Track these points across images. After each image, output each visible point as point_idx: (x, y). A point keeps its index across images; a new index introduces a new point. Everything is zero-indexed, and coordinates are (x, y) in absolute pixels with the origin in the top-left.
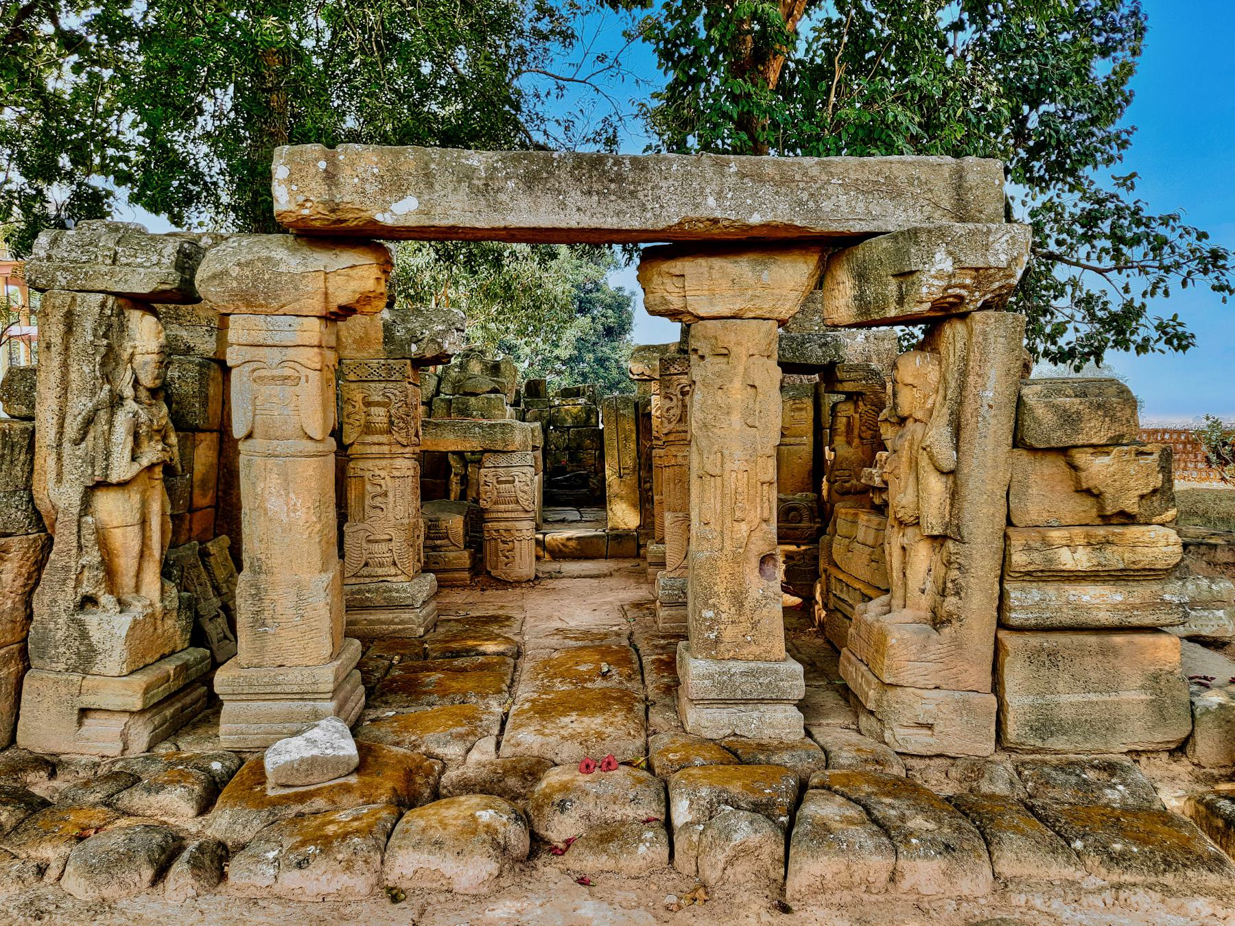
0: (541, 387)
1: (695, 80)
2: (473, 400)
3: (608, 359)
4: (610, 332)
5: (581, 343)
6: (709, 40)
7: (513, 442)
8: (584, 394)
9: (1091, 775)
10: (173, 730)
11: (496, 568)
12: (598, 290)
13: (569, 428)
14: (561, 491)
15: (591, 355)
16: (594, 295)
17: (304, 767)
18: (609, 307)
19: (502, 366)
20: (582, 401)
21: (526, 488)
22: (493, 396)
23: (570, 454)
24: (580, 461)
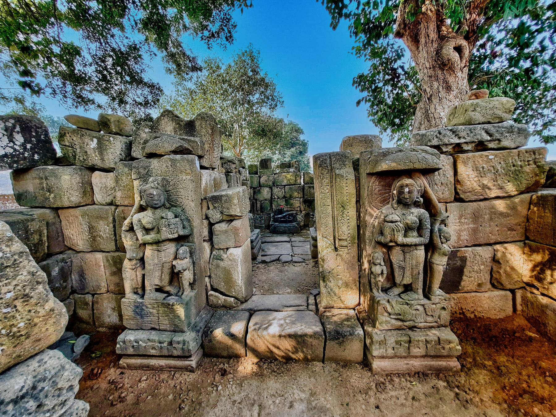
0: (268, 163)
1: (190, 61)
4: (301, 153)
6: (529, 93)
8: (293, 166)
9: (361, 321)
10: (54, 25)
13: (285, 186)
17: (402, 26)
19: (197, 124)
20: (292, 170)
22: (178, 157)
23: (286, 200)
24: (292, 204)
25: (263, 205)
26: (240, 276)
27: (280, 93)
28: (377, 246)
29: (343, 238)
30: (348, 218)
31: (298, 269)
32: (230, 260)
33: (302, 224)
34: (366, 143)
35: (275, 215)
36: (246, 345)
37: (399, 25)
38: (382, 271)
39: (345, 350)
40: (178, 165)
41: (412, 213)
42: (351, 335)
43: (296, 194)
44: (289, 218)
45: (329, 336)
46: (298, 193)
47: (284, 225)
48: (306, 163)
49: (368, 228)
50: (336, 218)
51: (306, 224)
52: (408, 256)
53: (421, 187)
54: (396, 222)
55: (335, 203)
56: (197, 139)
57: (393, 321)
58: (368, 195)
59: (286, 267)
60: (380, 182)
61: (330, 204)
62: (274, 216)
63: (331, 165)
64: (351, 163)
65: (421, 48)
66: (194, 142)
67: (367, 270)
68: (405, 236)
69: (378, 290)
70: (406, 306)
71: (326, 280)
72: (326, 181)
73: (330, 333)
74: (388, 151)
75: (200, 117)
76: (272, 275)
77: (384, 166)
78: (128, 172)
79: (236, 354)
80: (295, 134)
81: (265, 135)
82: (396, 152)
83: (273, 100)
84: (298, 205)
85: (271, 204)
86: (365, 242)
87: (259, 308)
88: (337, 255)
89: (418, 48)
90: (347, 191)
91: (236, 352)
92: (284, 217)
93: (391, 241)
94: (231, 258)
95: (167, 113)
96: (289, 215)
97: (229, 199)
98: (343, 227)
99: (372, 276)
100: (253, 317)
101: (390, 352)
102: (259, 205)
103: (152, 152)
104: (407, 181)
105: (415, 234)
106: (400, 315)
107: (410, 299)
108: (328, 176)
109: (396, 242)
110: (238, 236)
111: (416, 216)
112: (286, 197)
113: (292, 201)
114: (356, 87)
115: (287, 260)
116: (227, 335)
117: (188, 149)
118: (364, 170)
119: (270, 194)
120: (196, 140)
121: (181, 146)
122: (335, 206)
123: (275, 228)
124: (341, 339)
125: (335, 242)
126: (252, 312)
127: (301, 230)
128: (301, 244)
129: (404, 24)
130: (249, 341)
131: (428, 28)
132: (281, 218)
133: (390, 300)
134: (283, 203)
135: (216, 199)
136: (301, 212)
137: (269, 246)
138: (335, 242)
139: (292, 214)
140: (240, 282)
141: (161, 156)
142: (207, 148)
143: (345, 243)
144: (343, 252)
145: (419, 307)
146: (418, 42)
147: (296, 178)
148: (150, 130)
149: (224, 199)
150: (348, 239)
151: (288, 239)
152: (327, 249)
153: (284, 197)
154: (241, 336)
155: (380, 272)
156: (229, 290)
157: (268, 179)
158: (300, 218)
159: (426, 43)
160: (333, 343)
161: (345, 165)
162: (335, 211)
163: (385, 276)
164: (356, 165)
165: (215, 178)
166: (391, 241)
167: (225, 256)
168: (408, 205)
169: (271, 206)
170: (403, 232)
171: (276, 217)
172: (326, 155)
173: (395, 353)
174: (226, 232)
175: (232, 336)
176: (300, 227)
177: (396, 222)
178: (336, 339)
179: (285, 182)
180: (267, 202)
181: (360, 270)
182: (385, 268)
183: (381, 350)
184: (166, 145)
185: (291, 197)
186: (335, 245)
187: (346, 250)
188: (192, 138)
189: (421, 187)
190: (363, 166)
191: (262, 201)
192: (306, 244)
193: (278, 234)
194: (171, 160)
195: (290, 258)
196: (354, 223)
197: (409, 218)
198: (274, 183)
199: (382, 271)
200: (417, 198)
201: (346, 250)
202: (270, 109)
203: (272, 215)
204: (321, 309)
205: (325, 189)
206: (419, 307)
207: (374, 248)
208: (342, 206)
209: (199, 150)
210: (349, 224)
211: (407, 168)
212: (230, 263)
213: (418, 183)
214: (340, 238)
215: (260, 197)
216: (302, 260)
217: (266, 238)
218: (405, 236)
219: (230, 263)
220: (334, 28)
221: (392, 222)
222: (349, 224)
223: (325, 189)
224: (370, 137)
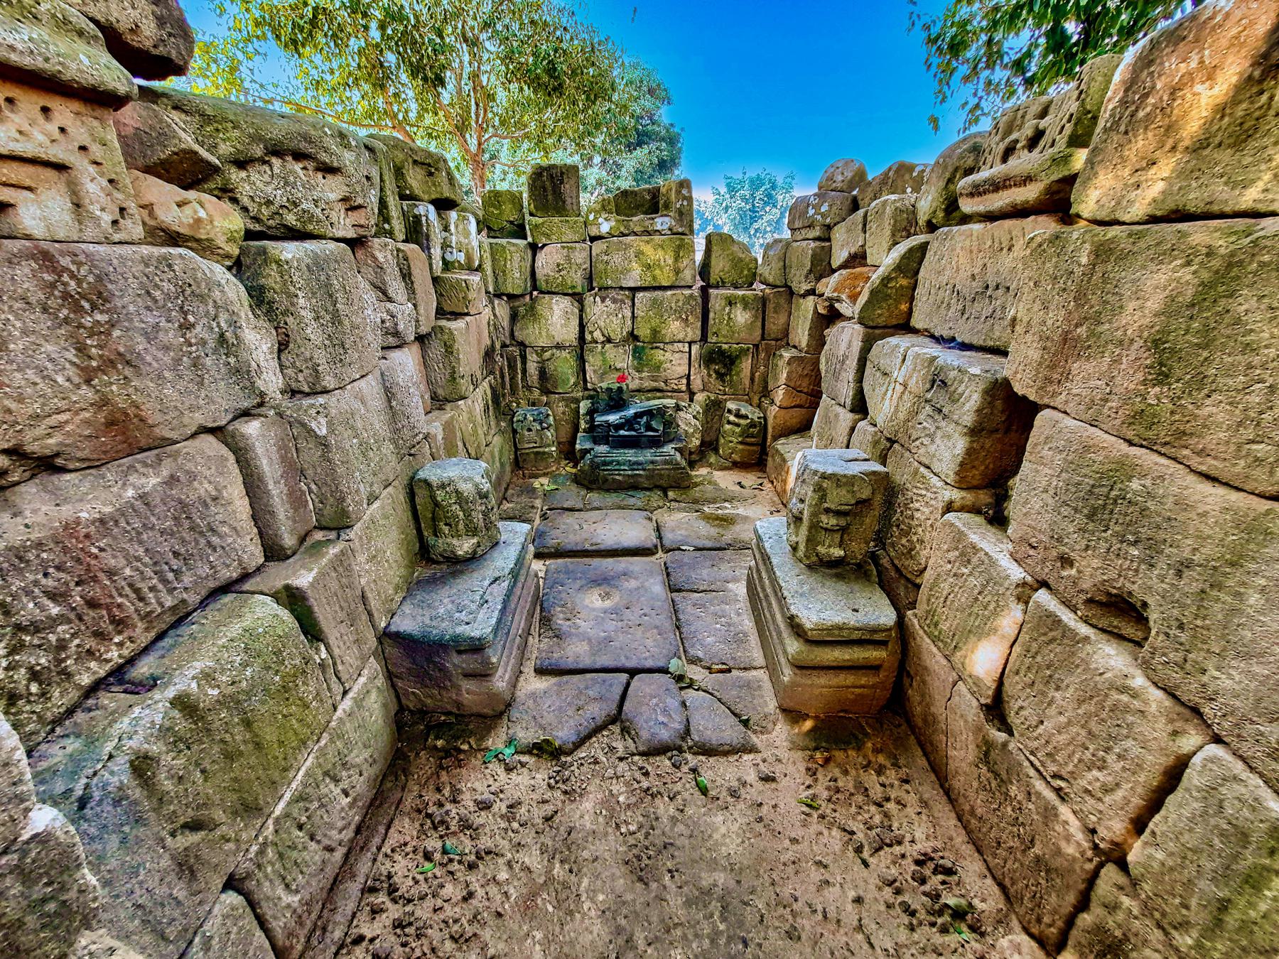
0: (567, 188)
13: (634, 290)
18: (663, 139)
25: (551, 367)
43: (674, 328)
47: (630, 455)
80: (647, 102)
81: (559, 89)
85: (582, 360)
92: (629, 423)
96: (649, 413)
102: (532, 367)
113: (659, 355)
132: (618, 427)
134: (622, 359)
139: (661, 411)
153: (633, 336)
157: (568, 258)
158: (689, 421)
171: (599, 419)
179: (634, 277)
180: (565, 354)
185: (656, 339)
191: (544, 349)
198: (590, 279)
215: (533, 334)
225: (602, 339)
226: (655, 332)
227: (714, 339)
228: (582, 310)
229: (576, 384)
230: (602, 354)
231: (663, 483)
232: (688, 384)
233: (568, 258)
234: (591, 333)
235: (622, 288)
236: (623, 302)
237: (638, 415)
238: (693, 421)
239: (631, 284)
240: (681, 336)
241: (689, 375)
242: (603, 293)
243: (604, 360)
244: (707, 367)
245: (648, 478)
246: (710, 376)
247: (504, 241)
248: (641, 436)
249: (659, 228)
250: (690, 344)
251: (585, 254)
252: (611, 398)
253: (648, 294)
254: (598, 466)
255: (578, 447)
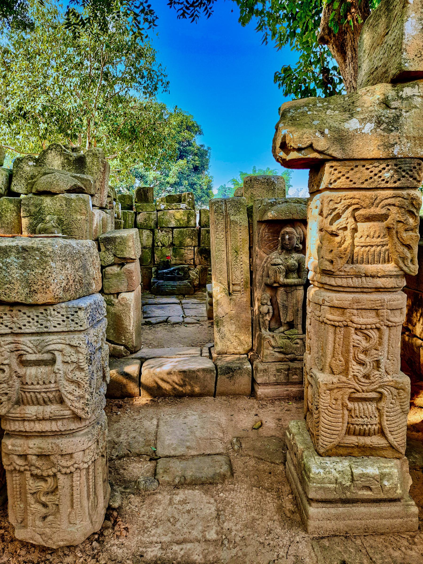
0: (149, 194)
2: (47, 201)
3: (195, 184)
5: (181, 175)
7: (46, 286)
11: (23, 524)
12: (190, 146)
13: (173, 228)
14: (166, 283)
15: (186, 182)
16: (188, 148)
17: (327, 31)
18: (196, 154)
19: (88, 160)
20: (183, 206)
21: (79, 375)
22: (73, 196)
24: (182, 255)
26: (132, 321)
27: (163, 67)
28: (267, 289)
29: (237, 283)
30: (241, 263)
31: (191, 329)
32: (121, 304)
33: (197, 282)
34: (268, 185)
35: (158, 269)
36: (140, 385)
37: (323, 30)
38: (269, 310)
39: (235, 383)
40: (73, 204)
41: (293, 257)
42: (240, 369)
43: (188, 241)
44: (178, 274)
45: (220, 371)
46: (192, 239)
47: (172, 283)
48: (205, 187)
49: (258, 272)
50: (230, 263)
51: (202, 283)
52: (290, 295)
53: (300, 235)
54: (279, 264)
55: (230, 249)
56: (90, 178)
57: (277, 354)
58: (258, 242)
59: (177, 328)
60: (269, 230)
61: (225, 249)
62: (156, 271)
63: (226, 211)
64: (246, 210)
65: (347, 61)
66: (86, 180)
67: (257, 311)
68: (286, 277)
69: (266, 328)
70: (287, 340)
71: (219, 324)
72: (221, 226)
73: (221, 368)
74: (275, 202)
75: (91, 153)
76: (159, 335)
77: (270, 215)
78: (13, 209)
79: (130, 394)
80: (186, 134)
82: (282, 203)
83: (151, 78)
84: (191, 256)
85: (153, 253)
86: (256, 285)
87: (151, 357)
88: (230, 300)
89: (345, 60)
90: (241, 237)
91: (130, 391)
92: (171, 272)
93: (275, 282)
94: (123, 303)
95: (54, 146)
96: (178, 269)
97: (124, 241)
98: (236, 272)
99: (261, 316)
100: (144, 365)
101: (273, 379)
103: (46, 189)
104: (288, 229)
105: (295, 275)
106: (282, 348)
107: (291, 333)
108: (223, 221)
109: (278, 283)
110: (132, 279)
111: (296, 260)
112: (174, 245)
113: (183, 251)
114: (279, 85)
115: (178, 321)
116: (122, 375)
117: (81, 188)
118: (256, 217)
119: (151, 239)
120: (89, 178)
121: (75, 185)
122: (230, 251)
123: (158, 287)
124: (231, 373)
125: (229, 287)
126: (143, 360)
127: (195, 291)
128: (195, 306)
129: (328, 30)
130: (143, 380)
131: (354, 41)
132: (167, 273)
133: (275, 336)
134: (169, 253)
135: (109, 241)
136: (195, 266)
137: (153, 308)
138: (229, 287)
139: (183, 269)
140: (131, 328)
141: (56, 194)
142: (98, 187)
143: (238, 288)
144: (237, 296)
145: (298, 341)
146: (345, 53)
147: (188, 218)
148: (35, 164)
149: (118, 240)
150: (241, 284)
151: (177, 301)
152: (221, 294)
153: (172, 244)
154: (135, 375)
155: (266, 311)
156: (119, 338)
157: (149, 217)
158: (193, 273)
159: (352, 57)
160: (224, 377)
161: (239, 212)
162: (230, 257)
163: (271, 314)
164: (250, 212)
165: (103, 219)
166: (275, 282)
167: (117, 301)
168: (290, 250)
169: (153, 257)
170: (284, 273)
171: (160, 272)
172: (221, 201)
173: (276, 380)
174: (118, 275)
175: (127, 375)
176: (194, 287)
177: (279, 264)
178: (227, 374)
179: (173, 224)
181: (252, 311)
182: (271, 307)
183: (265, 377)
184: (61, 184)
185: (182, 245)
186: (229, 290)
187: (240, 294)
188: (82, 176)
189: (300, 235)
190: (255, 214)
192: (201, 306)
193: (163, 295)
194: (66, 199)
195: (181, 319)
196: (246, 267)
197: (290, 261)
198: (156, 224)
199: (269, 310)
200: (297, 244)
201: (240, 294)
202: (145, 93)
203: (154, 269)
204: (214, 355)
205: (220, 234)
206: (298, 341)
207: (264, 291)
208: (236, 252)
209: (92, 189)
210: (242, 269)
211: (287, 218)
212: (121, 308)
213: (298, 231)
214: (233, 283)
216: (196, 321)
217: (147, 300)
218: (286, 277)
219: (121, 308)
220: (243, 24)
221: (275, 265)
222: (242, 269)
223: (220, 234)
224: (273, 179)
225: (161, 245)
226: (181, 243)
227: (203, 245)
228: (154, 234)
229: (151, 262)
230: (161, 250)
231: (183, 292)
232: (194, 262)
233: (149, 217)
234: (157, 243)
235: (168, 227)
236: (169, 232)
237: (174, 270)
238: (196, 274)
239: (172, 226)
240: (190, 244)
241: (194, 258)
242: (162, 229)
243: (162, 253)
244: (201, 255)
245: (178, 290)
246: (202, 258)
247: (126, 211)
248: (175, 277)
249: (182, 207)
250: (194, 247)
251: (155, 216)
252: (164, 264)
253: (178, 229)
254: (160, 286)
255: (152, 281)
